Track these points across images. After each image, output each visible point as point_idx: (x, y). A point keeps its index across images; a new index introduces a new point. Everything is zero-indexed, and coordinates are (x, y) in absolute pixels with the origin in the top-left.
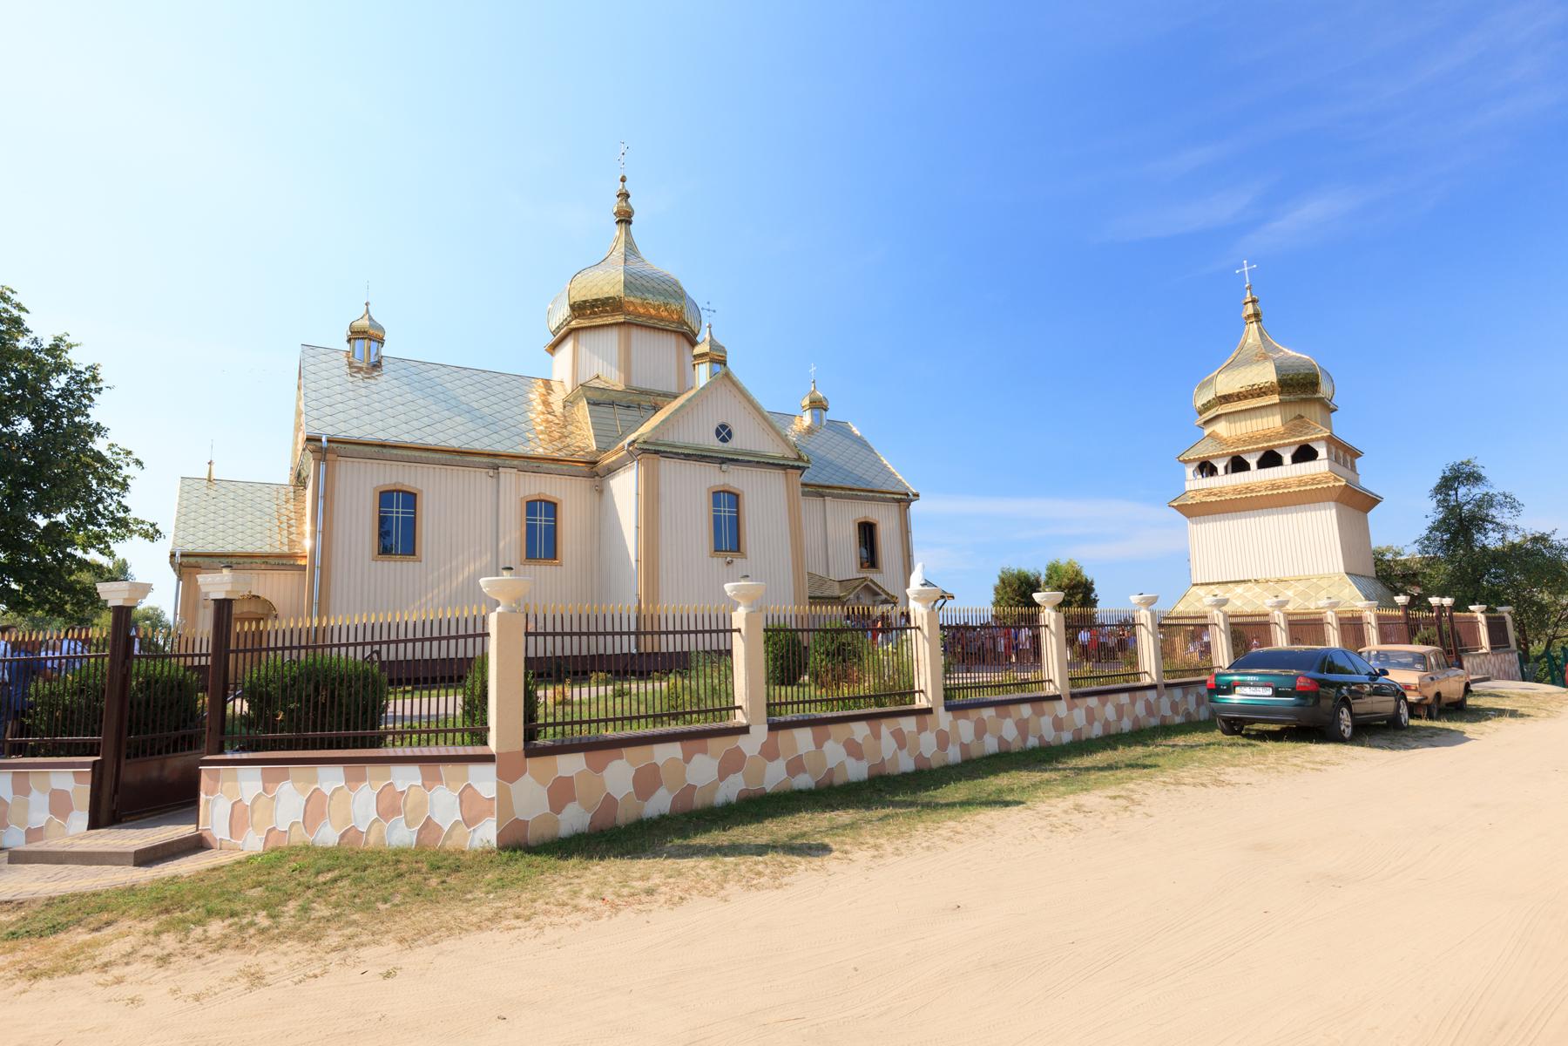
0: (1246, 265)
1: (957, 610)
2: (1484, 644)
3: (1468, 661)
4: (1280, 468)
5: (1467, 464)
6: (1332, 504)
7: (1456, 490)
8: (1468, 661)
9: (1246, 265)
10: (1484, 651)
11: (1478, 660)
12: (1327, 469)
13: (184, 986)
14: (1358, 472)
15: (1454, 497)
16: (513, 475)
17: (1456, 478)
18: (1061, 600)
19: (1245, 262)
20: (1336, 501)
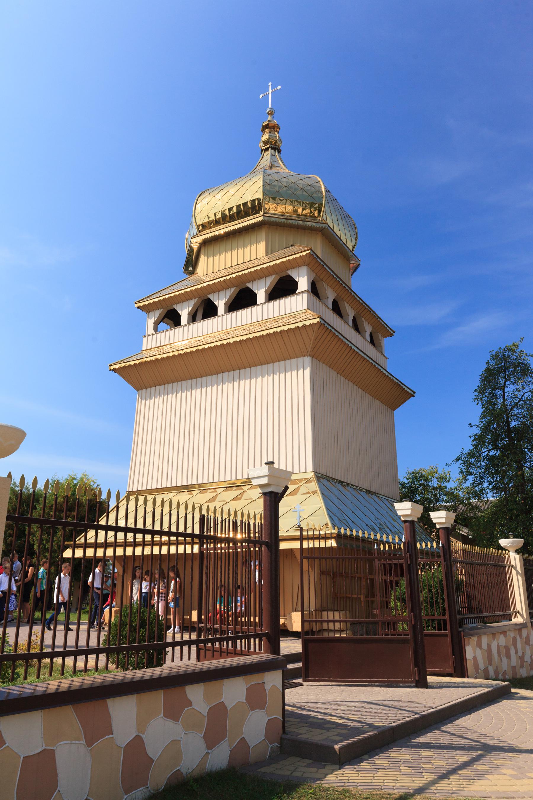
0: (270, 88)
1: (252, 516)
2: (519, 608)
3: (479, 645)
4: (254, 308)
5: (512, 349)
6: (307, 359)
7: (503, 388)
8: (479, 645)
9: (270, 88)
10: (518, 620)
11: (502, 640)
12: (305, 307)
13: (20, 672)
14: (385, 352)
15: (501, 400)
16: (296, 470)
17: (502, 370)
18: (521, 545)
19: (270, 84)
20: (313, 356)
